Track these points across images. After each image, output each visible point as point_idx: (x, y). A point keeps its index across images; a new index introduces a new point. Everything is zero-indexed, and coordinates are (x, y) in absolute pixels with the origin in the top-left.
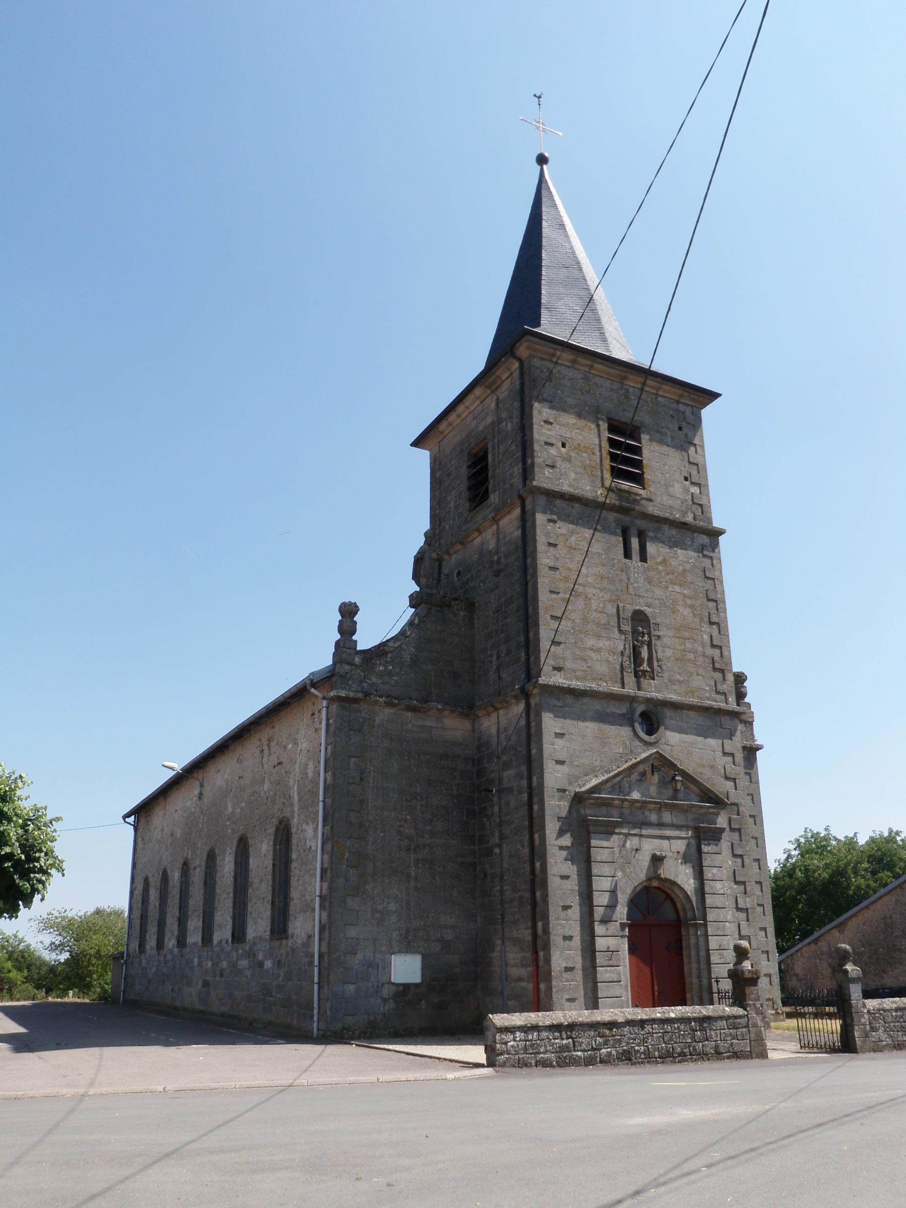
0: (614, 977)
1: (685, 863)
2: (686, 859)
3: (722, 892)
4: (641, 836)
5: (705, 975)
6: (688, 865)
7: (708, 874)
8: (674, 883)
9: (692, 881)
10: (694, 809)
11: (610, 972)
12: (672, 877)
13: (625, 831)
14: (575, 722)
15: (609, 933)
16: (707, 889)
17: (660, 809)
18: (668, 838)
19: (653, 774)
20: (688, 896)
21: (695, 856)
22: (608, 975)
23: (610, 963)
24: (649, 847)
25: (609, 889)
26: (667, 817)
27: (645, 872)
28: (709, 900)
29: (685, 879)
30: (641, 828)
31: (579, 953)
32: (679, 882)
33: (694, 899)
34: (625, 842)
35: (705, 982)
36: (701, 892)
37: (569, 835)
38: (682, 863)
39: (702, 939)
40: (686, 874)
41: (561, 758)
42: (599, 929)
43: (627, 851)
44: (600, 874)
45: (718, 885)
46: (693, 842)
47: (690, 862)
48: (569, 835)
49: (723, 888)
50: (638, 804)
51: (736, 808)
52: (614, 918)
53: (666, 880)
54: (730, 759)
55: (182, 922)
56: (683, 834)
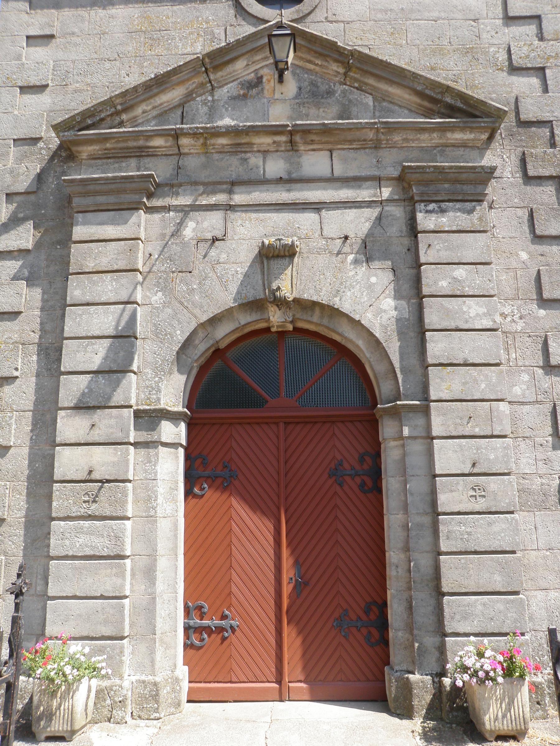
0: (102, 545)
1: (368, 260)
2: (369, 250)
3: (487, 323)
4: (230, 208)
5: (423, 542)
6: (376, 264)
7: (434, 280)
8: (334, 313)
9: (388, 304)
10: (397, 138)
11: (90, 532)
12: (323, 297)
13: (184, 200)
14: (81, 12)
15: (96, 436)
16: (432, 318)
17: (292, 145)
18: (317, 207)
19: (281, 79)
20: (378, 342)
21: (400, 244)
22: (82, 540)
23: (94, 509)
24: (250, 232)
25: (111, 331)
26: (315, 162)
27: (234, 288)
28: (437, 347)
29: (368, 300)
30: (230, 192)
31: (23, 486)
32: (346, 307)
33: (393, 349)
34: (180, 225)
35: (423, 561)
36: (416, 330)
37: (30, 225)
38: (356, 262)
39: (417, 447)
40: (370, 287)
41: (34, 80)
42: (69, 426)
43: (184, 245)
44: (88, 298)
45: (474, 311)
46: (397, 212)
47: (385, 256)
48: (30, 225)
49: (488, 314)
50: (223, 141)
51: (546, 132)
52: (117, 398)
53: (300, 303)
54: (531, 29)
55: (345, 527)
56: (365, 194)
